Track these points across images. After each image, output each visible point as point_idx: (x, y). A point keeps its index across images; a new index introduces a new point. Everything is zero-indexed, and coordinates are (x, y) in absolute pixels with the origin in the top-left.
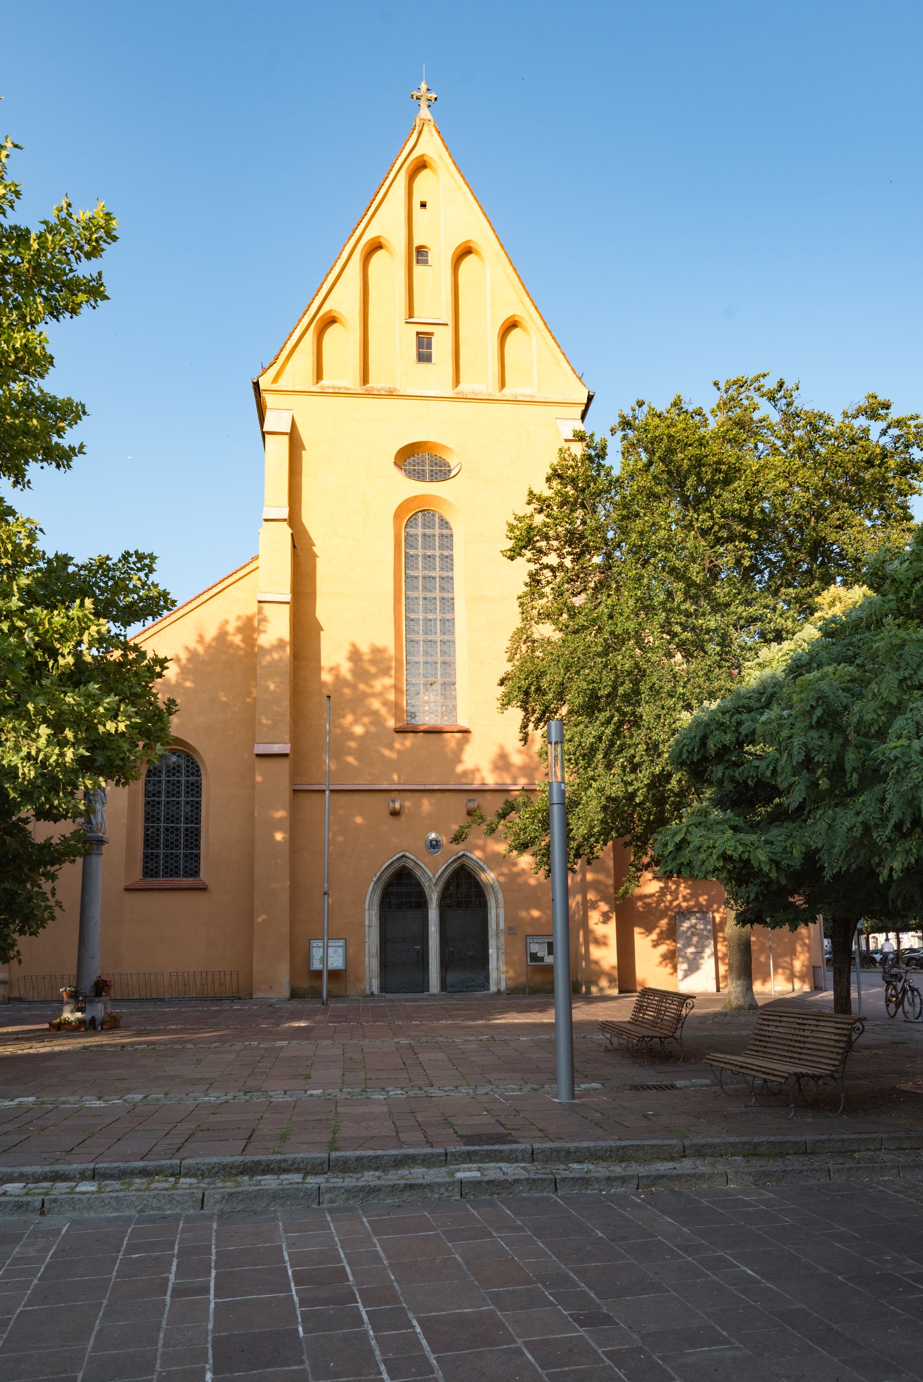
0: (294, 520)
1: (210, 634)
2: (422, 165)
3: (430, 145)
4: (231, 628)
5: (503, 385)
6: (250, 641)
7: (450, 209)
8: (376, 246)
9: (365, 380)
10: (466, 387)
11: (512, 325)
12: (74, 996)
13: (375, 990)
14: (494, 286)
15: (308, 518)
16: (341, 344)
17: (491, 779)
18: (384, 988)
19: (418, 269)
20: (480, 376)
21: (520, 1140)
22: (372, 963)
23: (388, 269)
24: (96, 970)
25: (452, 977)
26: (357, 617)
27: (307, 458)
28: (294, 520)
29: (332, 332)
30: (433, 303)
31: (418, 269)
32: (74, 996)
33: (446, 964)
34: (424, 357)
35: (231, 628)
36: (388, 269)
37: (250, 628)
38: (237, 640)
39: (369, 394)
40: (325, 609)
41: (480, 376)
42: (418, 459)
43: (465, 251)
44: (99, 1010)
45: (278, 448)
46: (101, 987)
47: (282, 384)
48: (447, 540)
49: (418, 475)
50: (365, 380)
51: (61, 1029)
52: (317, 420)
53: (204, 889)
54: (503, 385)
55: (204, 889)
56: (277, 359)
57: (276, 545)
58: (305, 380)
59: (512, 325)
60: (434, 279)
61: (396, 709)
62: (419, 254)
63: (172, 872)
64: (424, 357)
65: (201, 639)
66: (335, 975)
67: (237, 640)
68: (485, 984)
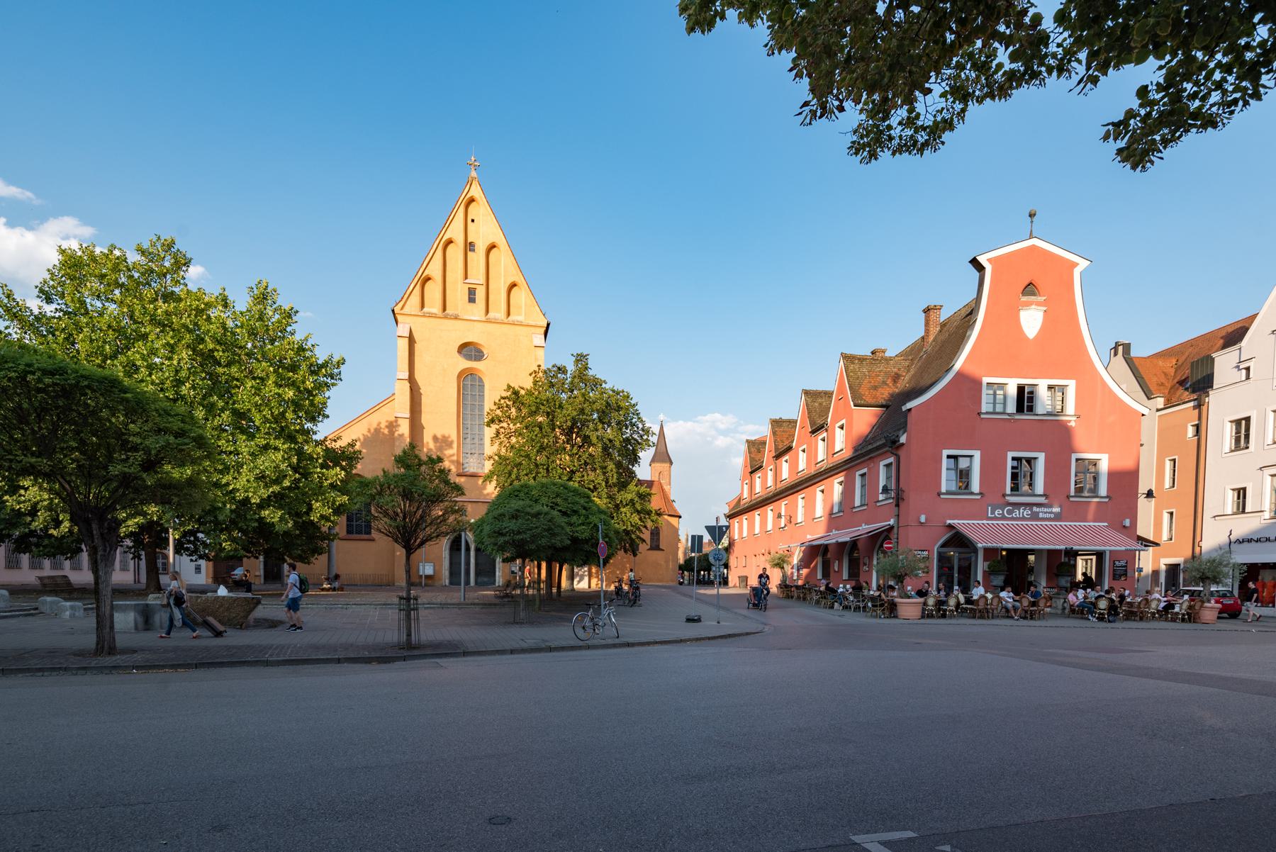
0: (412, 379)
1: (375, 426)
2: (472, 200)
3: (476, 191)
4: (383, 426)
5: (509, 314)
6: (392, 433)
7: (486, 228)
8: (450, 242)
9: (444, 309)
10: (491, 315)
11: (514, 285)
12: (327, 579)
13: (447, 582)
14: (505, 267)
15: (418, 377)
16: (433, 290)
17: (806, 80)
18: (451, 583)
19: (470, 254)
20: (498, 312)
21: (497, 601)
22: (445, 573)
23: (455, 253)
24: (334, 571)
25: (480, 580)
26: (440, 421)
27: (417, 347)
28: (412, 379)
29: (428, 284)
30: (477, 276)
31: (470, 254)
32: (327, 579)
33: (477, 574)
34: (472, 300)
35: (383, 426)
36: (455, 253)
37: (392, 426)
38: (386, 431)
39: (446, 317)
40: (426, 419)
41: (498, 312)
42: (469, 350)
43: (493, 246)
44: (336, 584)
45: (403, 345)
46: (337, 577)
47: (406, 310)
48: (482, 386)
49: (469, 357)
50: (444, 309)
51: (323, 590)
52: (422, 329)
53: (373, 540)
54: (509, 314)
55: (373, 540)
56: (405, 298)
57: (403, 391)
58: (416, 310)
59: (514, 285)
60: (477, 259)
61: (458, 463)
62: (469, 246)
63: (359, 532)
64: (472, 300)
65: (369, 431)
66: (428, 577)
67: (386, 431)
68: (494, 583)
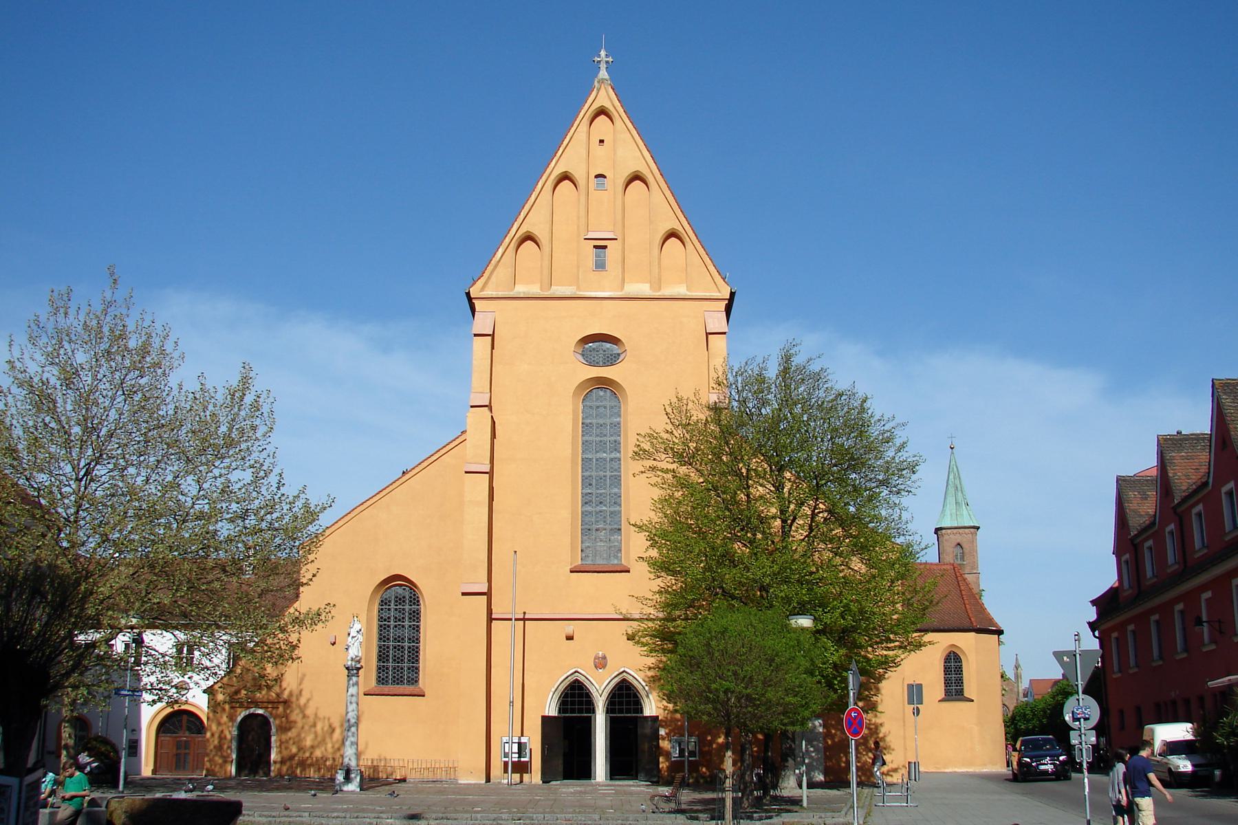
42: (599, 346)
